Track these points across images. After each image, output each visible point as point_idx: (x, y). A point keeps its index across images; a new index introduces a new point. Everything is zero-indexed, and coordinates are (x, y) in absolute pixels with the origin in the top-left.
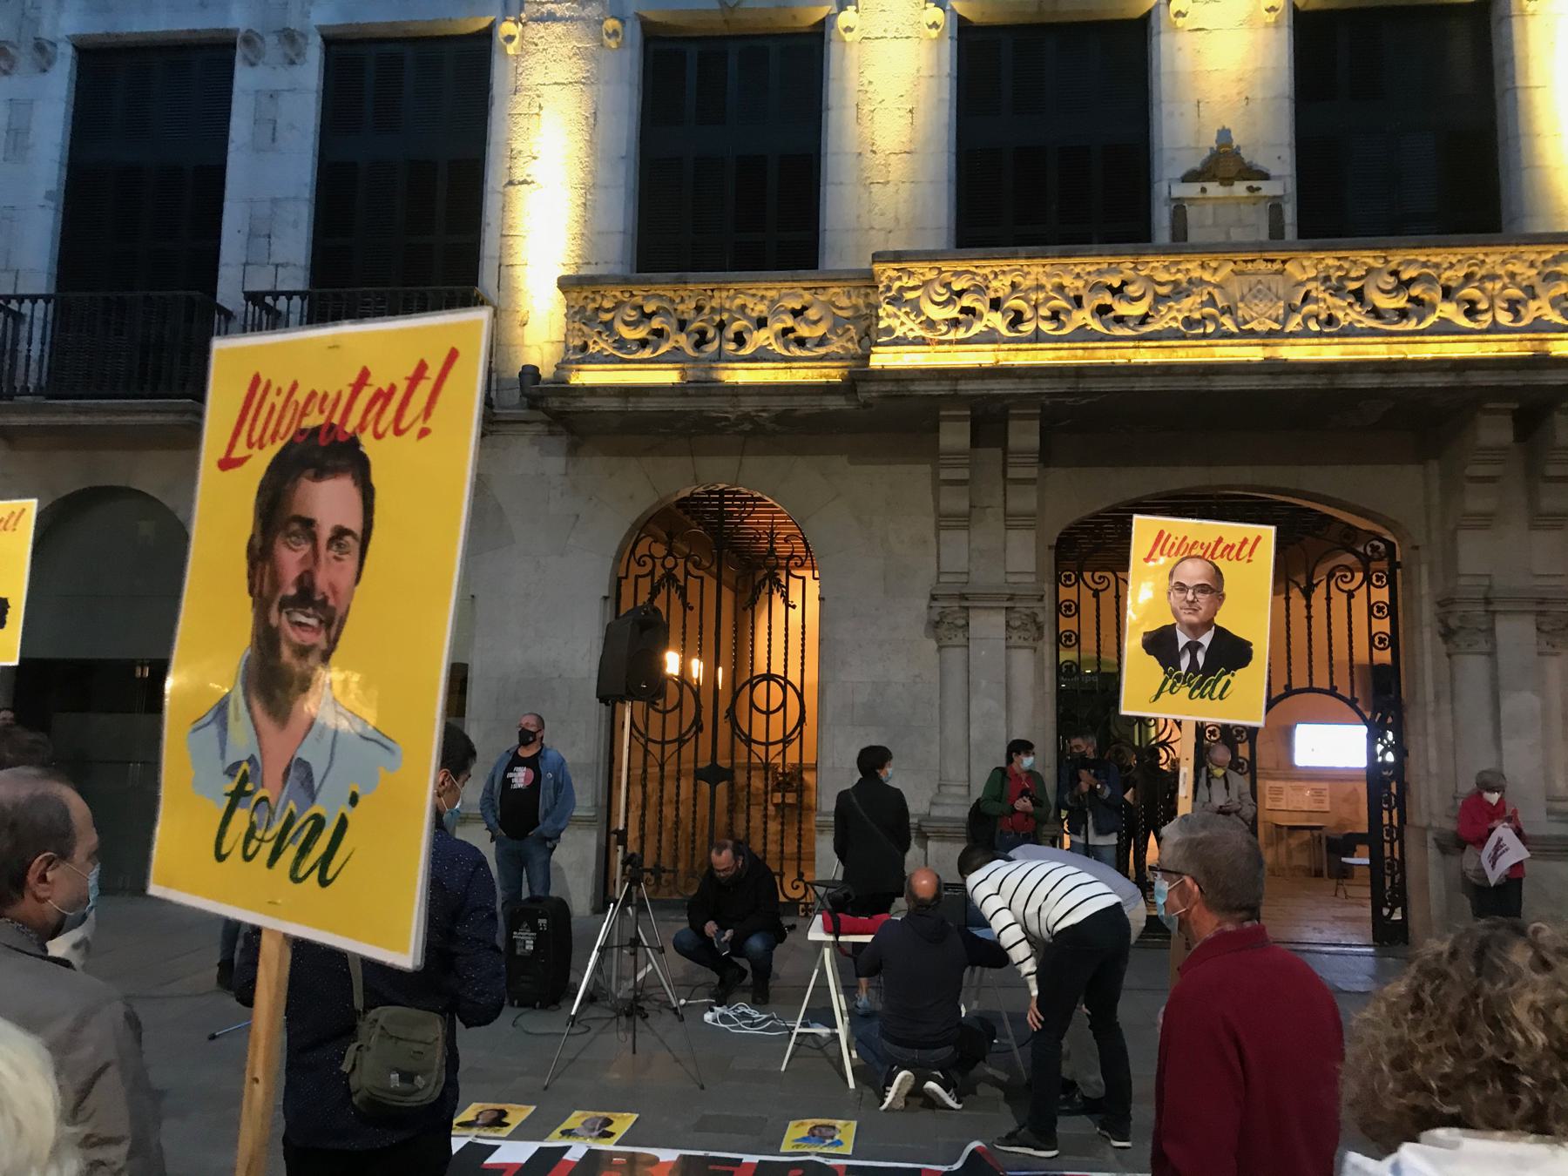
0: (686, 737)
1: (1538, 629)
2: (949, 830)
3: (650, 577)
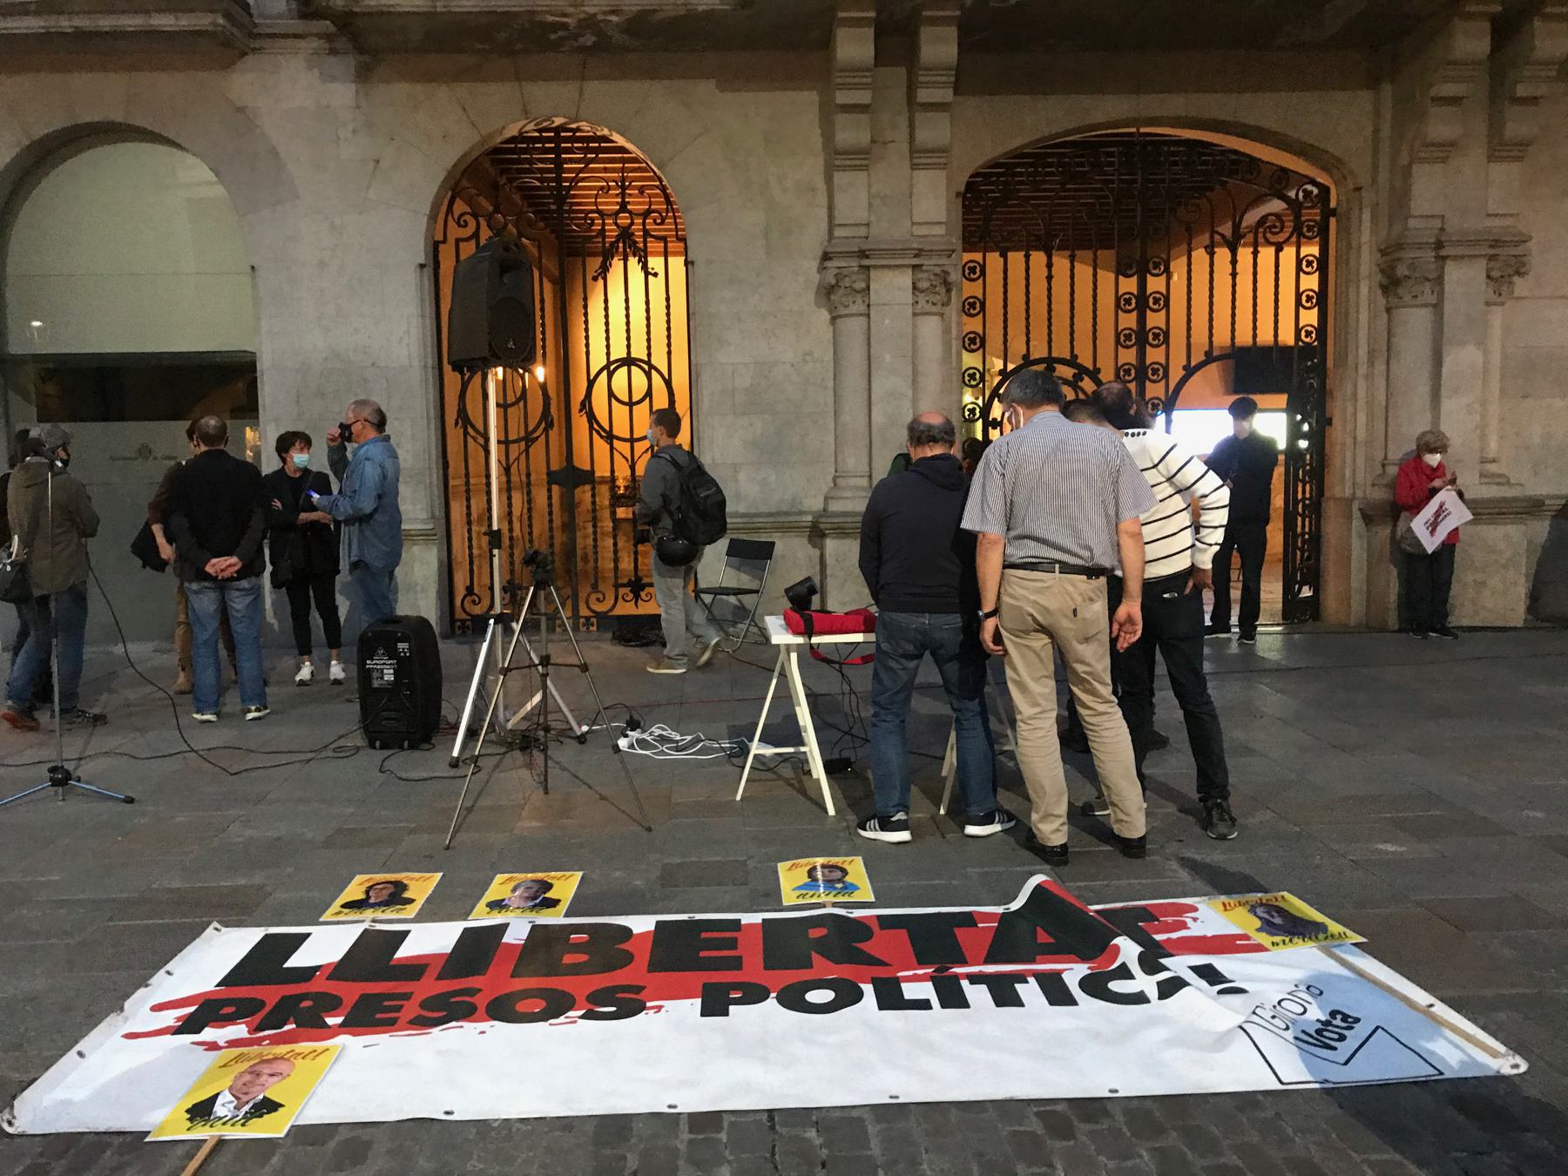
0: (535, 435)
1: (1488, 277)
2: (850, 525)
3: (474, 241)
